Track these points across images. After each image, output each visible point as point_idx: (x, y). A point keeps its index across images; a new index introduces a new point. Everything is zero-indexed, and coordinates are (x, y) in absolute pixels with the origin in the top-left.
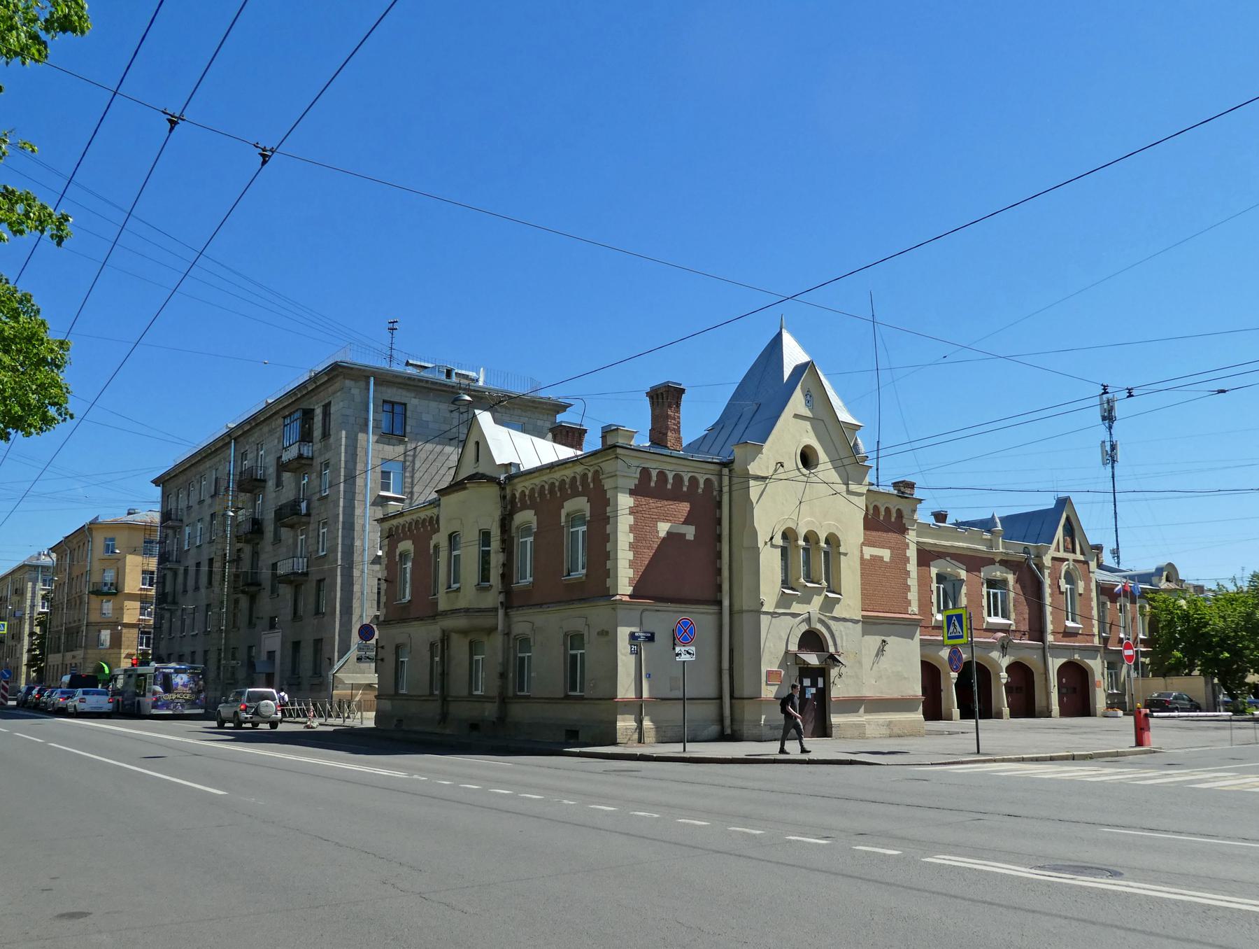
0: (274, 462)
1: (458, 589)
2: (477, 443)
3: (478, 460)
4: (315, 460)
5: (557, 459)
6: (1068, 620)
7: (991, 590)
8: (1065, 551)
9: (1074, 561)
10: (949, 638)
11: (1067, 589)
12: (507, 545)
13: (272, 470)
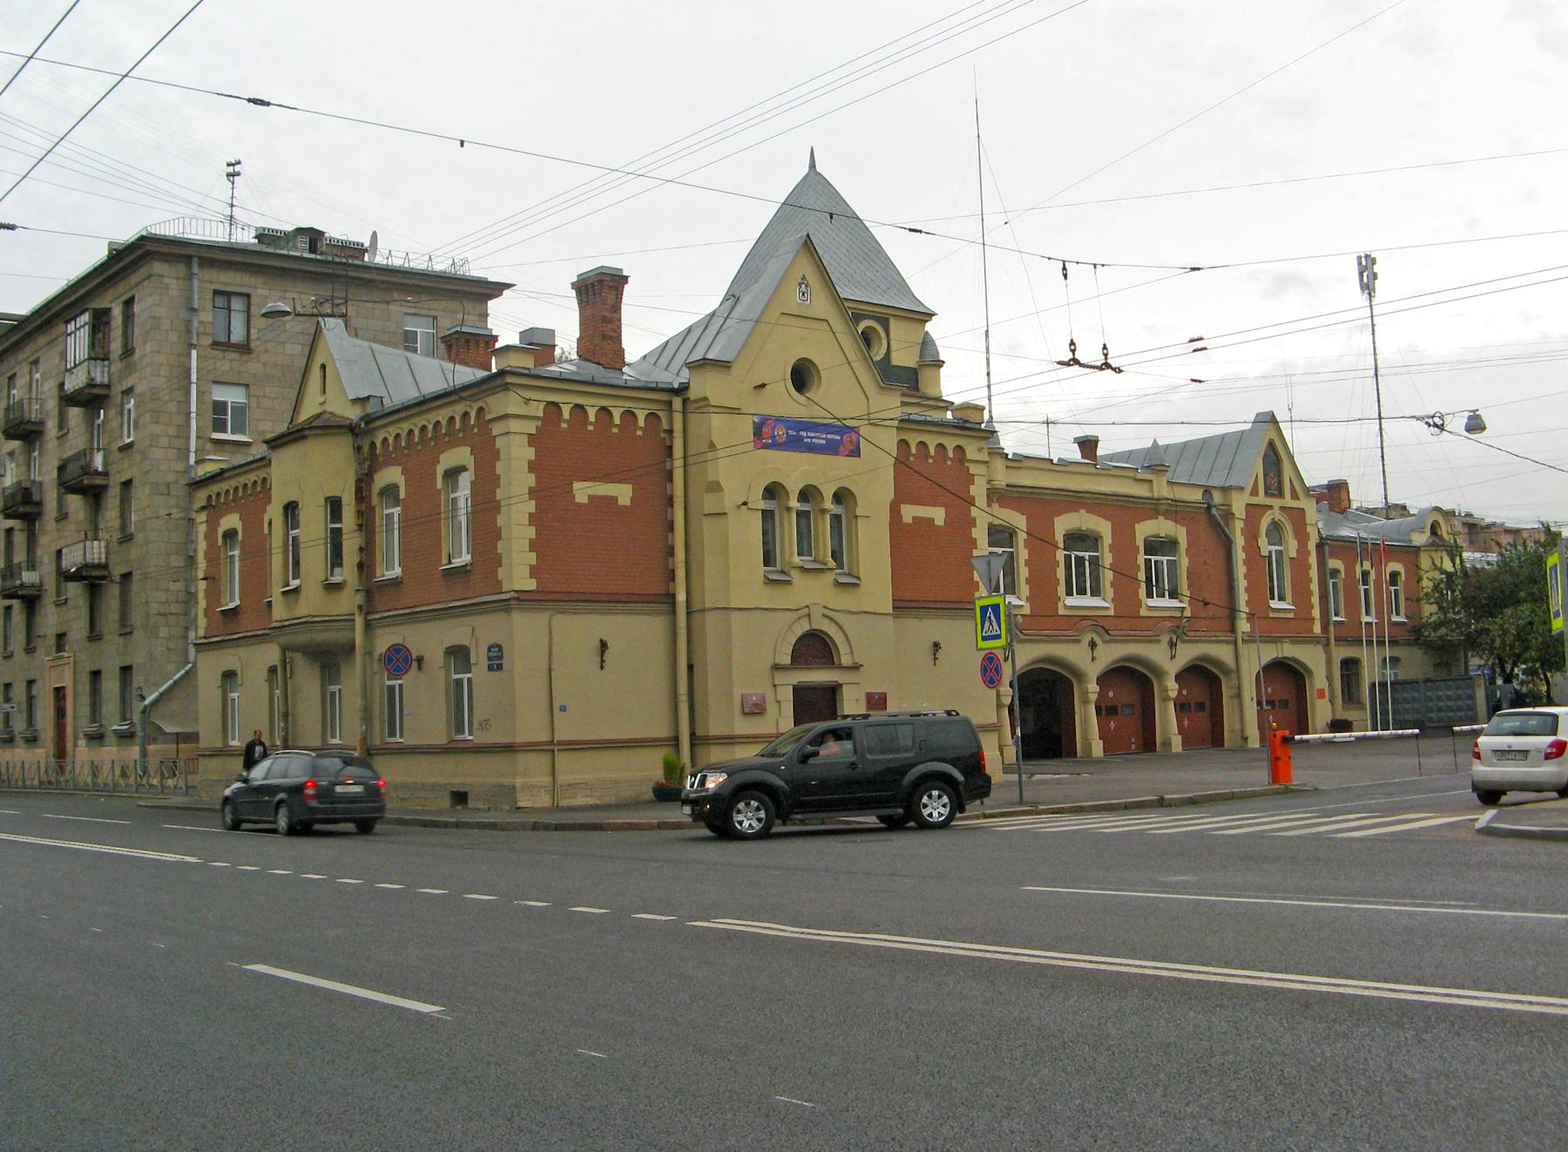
0: (55, 392)
1: (296, 590)
2: (323, 367)
3: (325, 393)
4: (113, 388)
5: (417, 394)
6: (1273, 598)
7: (1153, 558)
8: (1266, 494)
9: (1282, 508)
10: (984, 639)
11: (1270, 552)
12: (366, 522)
13: (52, 404)
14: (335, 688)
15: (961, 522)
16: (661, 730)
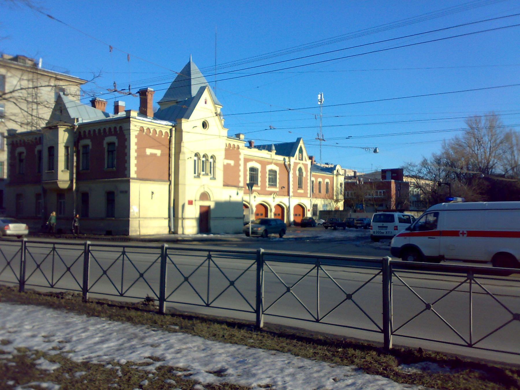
8: (299, 160)
9: (302, 164)
14: (62, 201)
15: (237, 165)
16: (141, 216)
